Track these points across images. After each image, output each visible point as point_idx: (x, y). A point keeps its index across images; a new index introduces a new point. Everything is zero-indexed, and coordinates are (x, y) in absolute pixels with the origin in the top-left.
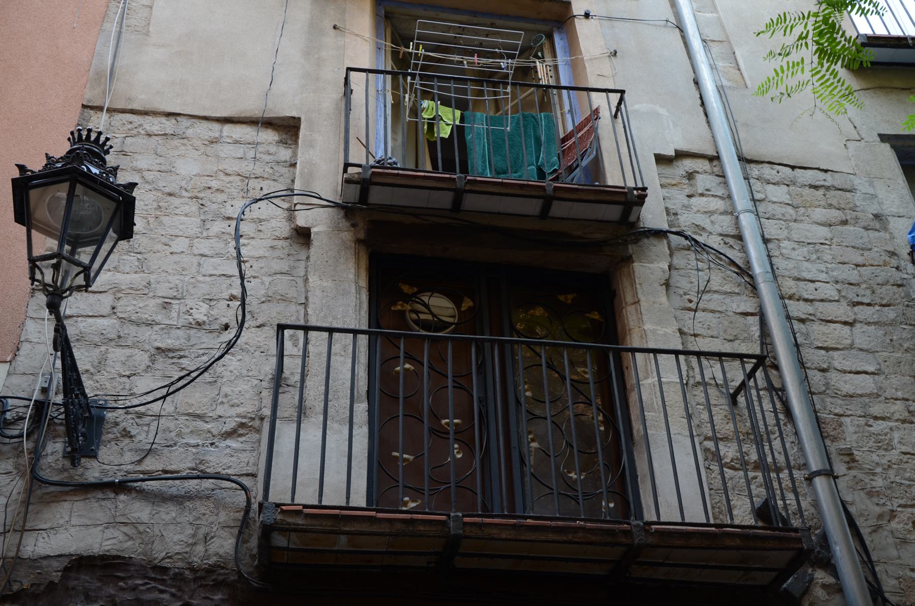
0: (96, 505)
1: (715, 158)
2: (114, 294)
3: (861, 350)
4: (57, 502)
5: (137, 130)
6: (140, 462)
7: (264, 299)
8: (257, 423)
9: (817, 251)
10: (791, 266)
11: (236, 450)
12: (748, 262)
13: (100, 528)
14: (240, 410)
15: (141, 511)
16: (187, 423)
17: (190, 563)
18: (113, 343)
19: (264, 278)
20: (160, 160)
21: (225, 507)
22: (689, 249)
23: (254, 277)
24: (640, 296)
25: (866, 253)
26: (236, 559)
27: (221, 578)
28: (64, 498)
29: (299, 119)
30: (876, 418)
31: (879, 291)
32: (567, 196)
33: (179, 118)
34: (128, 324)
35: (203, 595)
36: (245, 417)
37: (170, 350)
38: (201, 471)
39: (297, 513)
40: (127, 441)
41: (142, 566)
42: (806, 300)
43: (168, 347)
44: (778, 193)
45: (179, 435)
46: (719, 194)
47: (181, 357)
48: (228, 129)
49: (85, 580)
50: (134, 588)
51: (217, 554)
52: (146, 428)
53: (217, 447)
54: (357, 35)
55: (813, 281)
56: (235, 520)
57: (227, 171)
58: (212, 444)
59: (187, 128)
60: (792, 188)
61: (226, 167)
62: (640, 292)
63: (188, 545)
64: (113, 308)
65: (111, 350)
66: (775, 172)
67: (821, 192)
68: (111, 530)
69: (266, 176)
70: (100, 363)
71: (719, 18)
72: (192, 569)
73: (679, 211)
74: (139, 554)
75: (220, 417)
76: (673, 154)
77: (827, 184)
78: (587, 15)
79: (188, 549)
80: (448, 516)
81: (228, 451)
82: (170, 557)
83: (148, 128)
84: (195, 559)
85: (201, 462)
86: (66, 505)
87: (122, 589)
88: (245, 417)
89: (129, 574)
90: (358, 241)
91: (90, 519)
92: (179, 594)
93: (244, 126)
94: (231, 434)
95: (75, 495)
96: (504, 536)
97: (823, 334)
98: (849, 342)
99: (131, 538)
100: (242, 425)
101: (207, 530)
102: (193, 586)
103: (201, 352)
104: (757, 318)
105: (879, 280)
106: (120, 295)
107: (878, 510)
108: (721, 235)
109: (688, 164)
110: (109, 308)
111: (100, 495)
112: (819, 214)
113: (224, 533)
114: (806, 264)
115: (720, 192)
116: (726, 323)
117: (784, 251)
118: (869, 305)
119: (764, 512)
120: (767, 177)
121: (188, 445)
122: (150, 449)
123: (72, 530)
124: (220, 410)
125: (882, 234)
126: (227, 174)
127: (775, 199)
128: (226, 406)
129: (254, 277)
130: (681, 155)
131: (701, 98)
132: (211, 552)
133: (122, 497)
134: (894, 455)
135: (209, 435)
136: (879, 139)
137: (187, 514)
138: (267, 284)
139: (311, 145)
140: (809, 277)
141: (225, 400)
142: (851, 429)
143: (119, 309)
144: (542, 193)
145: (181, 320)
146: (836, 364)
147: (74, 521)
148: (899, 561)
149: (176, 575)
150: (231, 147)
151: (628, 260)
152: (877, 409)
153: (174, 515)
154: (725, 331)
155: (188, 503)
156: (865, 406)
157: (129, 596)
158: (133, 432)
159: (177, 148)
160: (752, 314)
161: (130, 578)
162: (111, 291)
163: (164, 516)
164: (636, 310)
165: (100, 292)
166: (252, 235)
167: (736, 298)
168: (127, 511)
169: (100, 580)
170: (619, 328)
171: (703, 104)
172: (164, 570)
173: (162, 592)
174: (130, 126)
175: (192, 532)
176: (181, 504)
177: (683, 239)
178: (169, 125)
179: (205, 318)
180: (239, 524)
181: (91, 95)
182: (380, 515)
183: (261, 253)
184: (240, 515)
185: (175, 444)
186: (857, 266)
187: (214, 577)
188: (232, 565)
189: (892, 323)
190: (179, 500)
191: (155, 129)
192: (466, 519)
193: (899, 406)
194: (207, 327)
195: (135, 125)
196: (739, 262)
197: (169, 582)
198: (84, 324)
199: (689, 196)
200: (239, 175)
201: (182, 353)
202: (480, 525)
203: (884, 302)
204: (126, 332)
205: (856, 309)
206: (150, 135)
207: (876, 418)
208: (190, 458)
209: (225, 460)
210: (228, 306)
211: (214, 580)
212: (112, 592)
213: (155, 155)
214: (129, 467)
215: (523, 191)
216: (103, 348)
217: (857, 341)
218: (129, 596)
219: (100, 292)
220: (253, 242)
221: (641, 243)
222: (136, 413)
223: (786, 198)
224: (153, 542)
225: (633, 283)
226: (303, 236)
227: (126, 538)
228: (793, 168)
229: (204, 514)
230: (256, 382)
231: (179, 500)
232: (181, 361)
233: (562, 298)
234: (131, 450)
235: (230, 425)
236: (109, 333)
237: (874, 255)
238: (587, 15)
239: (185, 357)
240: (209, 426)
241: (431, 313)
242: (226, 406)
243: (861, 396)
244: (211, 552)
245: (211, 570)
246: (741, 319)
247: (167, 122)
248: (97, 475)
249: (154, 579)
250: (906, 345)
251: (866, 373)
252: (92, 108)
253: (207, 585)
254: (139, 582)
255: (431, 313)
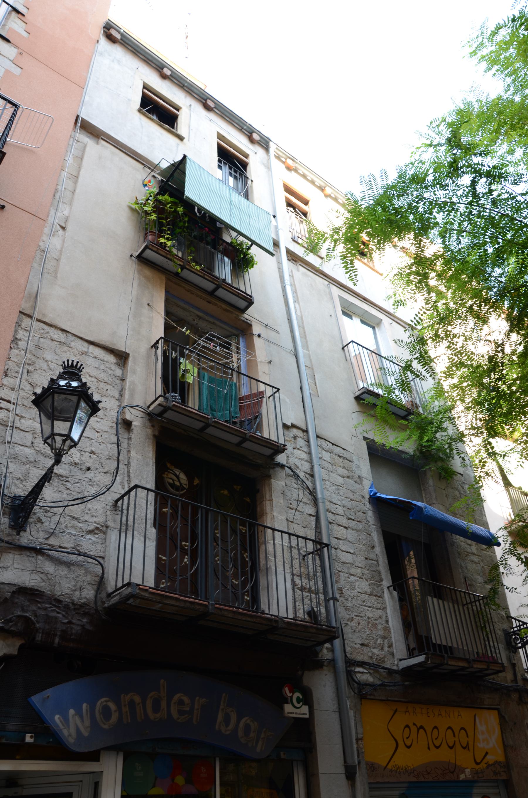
0: (26, 559)
1: (306, 431)
2: (33, 434)
3: (349, 541)
4: (6, 552)
5: (46, 335)
6: (47, 539)
7: (107, 457)
8: (104, 529)
9: (338, 489)
10: (329, 495)
11: (95, 542)
12: (315, 489)
13: (28, 572)
14: (97, 520)
15: (49, 567)
16: (70, 521)
17: (73, 600)
18: (32, 464)
19: (108, 444)
20: (57, 357)
21: (90, 573)
22: (292, 477)
23: (103, 443)
24: (273, 497)
25: (355, 495)
26: (96, 602)
27: (87, 611)
28: (9, 551)
29: (129, 354)
30: (351, 575)
31: (357, 514)
32: (254, 440)
33: (68, 334)
34: (40, 455)
35: (78, 618)
36: (98, 524)
37: (61, 476)
38: (78, 550)
39: (146, 590)
40: (40, 525)
41: (49, 597)
42: (333, 513)
43: (61, 474)
44: (326, 456)
45: (66, 527)
46: (305, 450)
47: (66, 481)
48: (91, 347)
49: (21, 599)
50: (45, 609)
51: (85, 598)
52: (49, 519)
53: (85, 538)
54: (158, 313)
55: (336, 504)
56: (95, 581)
57: (90, 374)
58: (82, 536)
59: (71, 341)
60: (332, 455)
61: (90, 371)
62: (273, 495)
63: (72, 591)
64: (32, 443)
65: (31, 468)
66: (326, 445)
67: (341, 460)
68: (34, 575)
69: (109, 382)
70: (26, 475)
71: (309, 354)
72: (73, 604)
73: (290, 456)
74: (48, 591)
75: (86, 521)
76: (290, 425)
77: (344, 456)
78: (259, 336)
79: (72, 593)
80: (209, 602)
81: (90, 541)
82: (63, 595)
83: (52, 335)
84: (75, 599)
85: (78, 545)
86: (11, 556)
87: (39, 608)
88: (98, 524)
89: (43, 601)
90: (154, 436)
91: (23, 566)
92: (67, 615)
93: (100, 349)
94: (91, 532)
95: (15, 551)
96: (229, 616)
97: (337, 531)
98: (345, 537)
99: (44, 581)
100: (97, 528)
101: (82, 584)
102: (73, 613)
103: (77, 481)
104: (315, 518)
105: (358, 509)
106: (36, 436)
107: (348, 617)
108: (304, 472)
109: (295, 432)
110: (30, 442)
111: (29, 554)
112: (341, 471)
113: (89, 587)
114: (334, 495)
115: (306, 449)
116: (303, 518)
117: (327, 486)
118: (354, 520)
119: (312, 614)
120: (324, 447)
121: (71, 534)
122: (53, 533)
123: (15, 570)
124: (86, 517)
125: (360, 486)
126: (90, 376)
127: (325, 459)
128: (89, 516)
129: (103, 443)
130: (293, 426)
131: (302, 397)
132: (83, 596)
133: (40, 557)
134: (355, 593)
135: (80, 530)
136: (362, 438)
137: (72, 573)
138: (109, 448)
139: (134, 372)
140: (334, 502)
141: (89, 512)
142: (343, 579)
143: (35, 445)
144: (244, 436)
145: (67, 459)
146: (340, 547)
147: (15, 565)
148: (352, 640)
149: (65, 605)
150: (92, 360)
151: (269, 477)
152: (352, 571)
153: (66, 573)
154: (303, 522)
155: (72, 567)
156: (348, 568)
157: (43, 613)
158: (43, 520)
159: (65, 352)
160: (313, 516)
161: (43, 603)
162: (31, 432)
163: (61, 573)
164: (270, 504)
165: (26, 432)
166: (102, 417)
167: (308, 506)
168: (42, 566)
169: (29, 601)
170: (259, 509)
171: (303, 401)
172: (60, 601)
173: (58, 613)
174: (43, 331)
175: (75, 584)
176: (69, 567)
177: (290, 471)
178: (62, 337)
179: (78, 461)
180: (97, 583)
181: (26, 307)
182: (182, 598)
183: (106, 429)
184: (97, 579)
185: (64, 532)
186: (351, 500)
187: (83, 610)
188: (92, 605)
189: (360, 531)
190: (68, 564)
191: (56, 337)
192: (216, 606)
193: (359, 571)
194: (79, 467)
195: (45, 331)
196: (311, 488)
197: (62, 608)
198: (18, 449)
199: (294, 449)
200: (96, 378)
201: (67, 479)
202: (221, 609)
203: (359, 520)
204: (39, 459)
205: (349, 521)
206: (52, 340)
207: (351, 575)
208: (72, 541)
209: (90, 547)
210: (90, 456)
211: (83, 611)
212: (35, 609)
213: (54, 354)
214: (42, 540)
215: (236, 433)
216: (27, 466)
217: (348, 537)
218: (43, 613)
219: (26, 432)
220: (102, 421)
221: (275, 470)
222: (45, 509)
223: (329, 459)
224: (55, 586)
225: (270, 490)
226: (127, 425)
227: (42, 581)
228: (333, 444)
229: (80, 575)
230: (104, 505)
231: (68, 564)
232: (67, 483)
233: (235, 487)
234: (42, 531)
235: (91, 527)
236: (30, 458)
237: (357, 497)
238: (259, 336)
239: (69, 482)
240: (81, 525)
241: (179, 482)
242: (89, 516)
243: (347, 563)
244: (83, 596)
245: (82, 605)
246: (308, 517)
247: (61, 335)
248: (26, 541)
249: (55, 606)
250: (364, 542)
251: (350, 553)
252: (24, 314)
253: (80, 613)
254: (47, 606)
255: (179, 482)
